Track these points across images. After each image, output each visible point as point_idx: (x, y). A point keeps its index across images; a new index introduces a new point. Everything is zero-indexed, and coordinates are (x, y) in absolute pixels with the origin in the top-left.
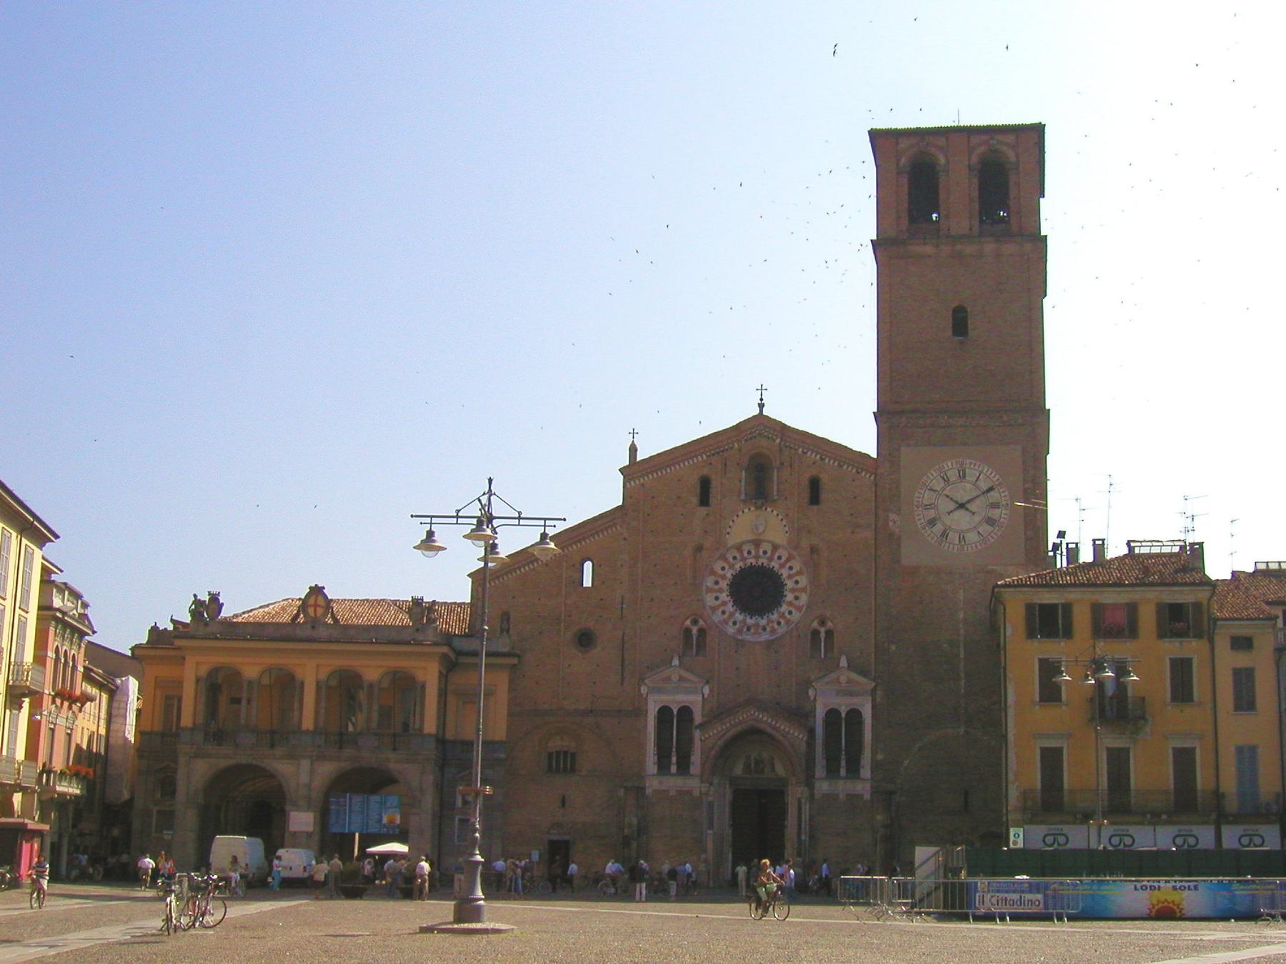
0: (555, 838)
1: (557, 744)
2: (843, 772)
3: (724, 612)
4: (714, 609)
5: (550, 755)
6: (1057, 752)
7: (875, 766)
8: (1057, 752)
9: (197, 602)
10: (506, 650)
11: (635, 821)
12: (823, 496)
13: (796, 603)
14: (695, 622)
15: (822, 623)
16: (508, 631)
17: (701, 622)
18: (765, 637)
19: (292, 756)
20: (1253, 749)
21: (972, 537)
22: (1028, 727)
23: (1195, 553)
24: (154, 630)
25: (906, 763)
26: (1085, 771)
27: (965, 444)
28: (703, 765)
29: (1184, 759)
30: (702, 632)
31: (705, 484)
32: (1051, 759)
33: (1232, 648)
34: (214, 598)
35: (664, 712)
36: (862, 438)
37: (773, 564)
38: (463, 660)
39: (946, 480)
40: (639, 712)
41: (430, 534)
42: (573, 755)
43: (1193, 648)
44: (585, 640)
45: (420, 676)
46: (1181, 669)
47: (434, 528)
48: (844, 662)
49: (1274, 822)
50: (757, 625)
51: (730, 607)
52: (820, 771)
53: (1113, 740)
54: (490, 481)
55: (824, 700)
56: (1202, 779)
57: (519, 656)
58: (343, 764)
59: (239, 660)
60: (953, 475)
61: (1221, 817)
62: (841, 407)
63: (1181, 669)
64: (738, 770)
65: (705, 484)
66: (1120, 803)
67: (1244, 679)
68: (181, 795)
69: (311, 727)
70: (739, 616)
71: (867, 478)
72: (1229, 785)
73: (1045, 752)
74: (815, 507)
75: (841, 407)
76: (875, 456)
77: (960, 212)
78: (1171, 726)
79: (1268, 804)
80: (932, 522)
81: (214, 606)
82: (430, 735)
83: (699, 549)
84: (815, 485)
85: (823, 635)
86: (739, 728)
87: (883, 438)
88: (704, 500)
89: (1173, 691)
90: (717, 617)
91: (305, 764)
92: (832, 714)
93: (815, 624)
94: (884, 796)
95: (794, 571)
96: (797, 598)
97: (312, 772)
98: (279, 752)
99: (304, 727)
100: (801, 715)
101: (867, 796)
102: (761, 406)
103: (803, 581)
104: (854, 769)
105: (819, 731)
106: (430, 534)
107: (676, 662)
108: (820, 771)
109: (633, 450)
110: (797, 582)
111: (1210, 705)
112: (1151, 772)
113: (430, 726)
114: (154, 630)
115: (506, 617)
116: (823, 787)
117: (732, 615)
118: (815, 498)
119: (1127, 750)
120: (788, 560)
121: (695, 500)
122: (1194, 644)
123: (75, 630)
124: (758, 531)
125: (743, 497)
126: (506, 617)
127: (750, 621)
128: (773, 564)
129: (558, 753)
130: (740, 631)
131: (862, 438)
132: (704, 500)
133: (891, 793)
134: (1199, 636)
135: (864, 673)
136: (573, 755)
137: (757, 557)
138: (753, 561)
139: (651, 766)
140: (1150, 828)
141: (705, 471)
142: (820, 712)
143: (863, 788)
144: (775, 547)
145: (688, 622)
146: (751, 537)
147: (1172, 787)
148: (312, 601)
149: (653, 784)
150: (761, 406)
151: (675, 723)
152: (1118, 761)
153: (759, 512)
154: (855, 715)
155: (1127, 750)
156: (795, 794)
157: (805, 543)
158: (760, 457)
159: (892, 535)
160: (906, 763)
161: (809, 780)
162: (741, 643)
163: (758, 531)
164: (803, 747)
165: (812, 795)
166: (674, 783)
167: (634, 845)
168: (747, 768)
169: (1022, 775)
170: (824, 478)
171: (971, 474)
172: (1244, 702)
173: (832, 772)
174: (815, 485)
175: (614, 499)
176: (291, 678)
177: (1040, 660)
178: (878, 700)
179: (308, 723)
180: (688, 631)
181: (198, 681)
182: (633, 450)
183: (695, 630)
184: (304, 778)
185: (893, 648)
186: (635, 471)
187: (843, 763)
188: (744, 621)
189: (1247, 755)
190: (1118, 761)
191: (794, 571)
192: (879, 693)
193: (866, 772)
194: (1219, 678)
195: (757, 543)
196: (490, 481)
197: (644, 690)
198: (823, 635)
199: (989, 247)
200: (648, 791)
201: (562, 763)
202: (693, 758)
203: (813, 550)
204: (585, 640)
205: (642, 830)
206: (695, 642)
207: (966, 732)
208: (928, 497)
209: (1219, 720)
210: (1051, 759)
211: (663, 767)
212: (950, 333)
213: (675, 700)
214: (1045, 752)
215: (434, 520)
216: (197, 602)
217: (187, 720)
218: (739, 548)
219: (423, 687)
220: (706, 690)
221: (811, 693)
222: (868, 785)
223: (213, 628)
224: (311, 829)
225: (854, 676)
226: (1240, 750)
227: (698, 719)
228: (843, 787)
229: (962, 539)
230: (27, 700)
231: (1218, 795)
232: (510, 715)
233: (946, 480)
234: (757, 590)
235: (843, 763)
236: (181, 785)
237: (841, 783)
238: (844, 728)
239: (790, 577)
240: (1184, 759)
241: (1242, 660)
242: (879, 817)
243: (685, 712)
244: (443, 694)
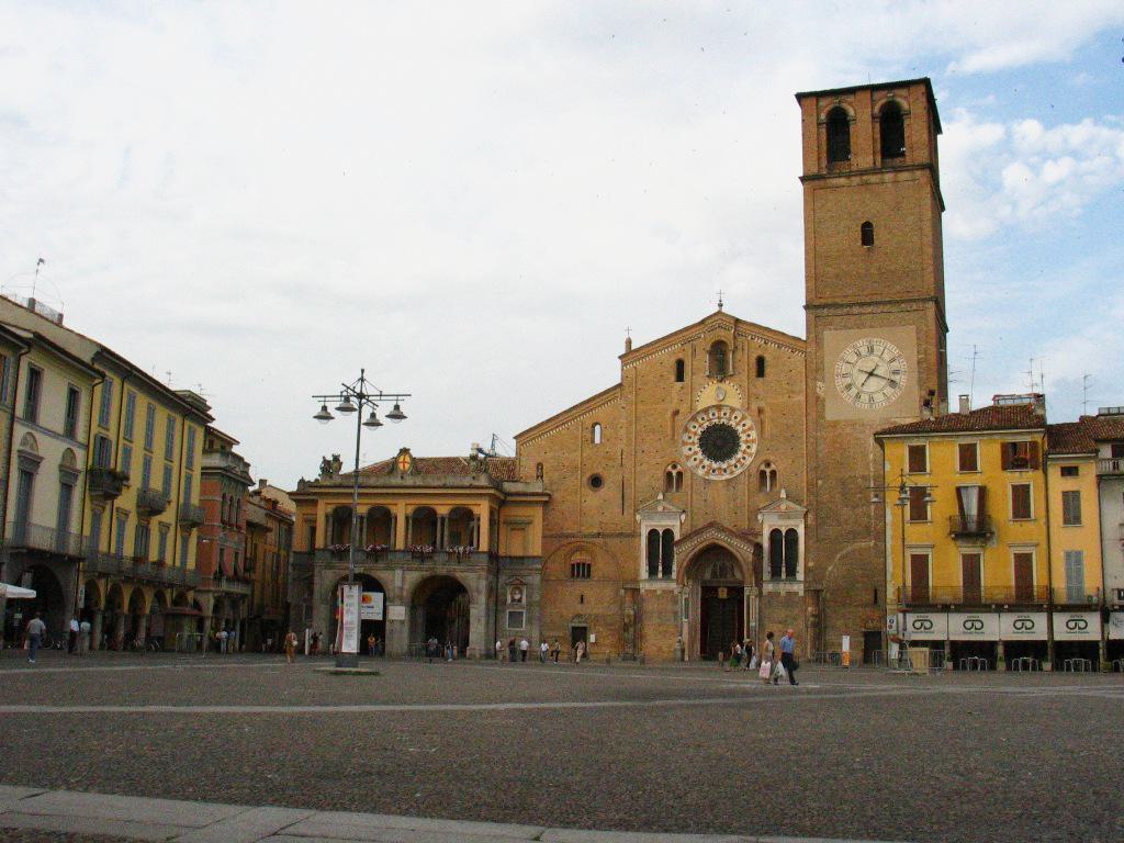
0: (577, 625)
1: (577, 558)
2: (783, 576)
3: (695, 459)
4: (688, 458)
5: (573, 565)
6: (1028, 556)
7: (807, 570)
8: (1028, 556)
9: (325, 462)
10: (540, 491)
11: (632, 613)
12: (767, 370)
13: (748, 451)
14: (674, 467)
15: (768, 465)
16: (542, 477)
17: (679, 467)
18: (727, 476)
19: (390, 568)
20: (1079, 554)
21: (879, 397)
22: (902, 540)
23: (210, 408)
24: (302, 482)
25: (830, 569)
26: (947, 574)
27: (871, 327)
28: (678, 573)
29: (1023, 563)
30: (680, 474)
31: (680, 364)
32: (920, 564)
33: (1063, 475)
34: (336, 458)
35: (653, 533)
36: (794, 323)
37: (731, 422)
38: (509, 498)
39: (859, 354)
40: (635, 535)
41: (397, 407)
42: (589, 565)
43: (1028, 477)
44: (596, 482)
45: (476, 510)
46: (1021, 494)
47: (327, 404)
48: (783, 495)
49: (1095, 611)
50: (720, 469)
51: (700, 456)
52: (766, 576)
53: (969, 550)
54: (363, 371)
55: (768, 523)
56: (1038, 579)
57: (549, 495)
58: (424, 573)
59: (389, 501)
60: (864, 351)
61: (1052, 608)
62: (778, 302)
63: (1021, 494)
64: (708, 576)
65: (680, 364)
66: (972, 601)
67: (1071, 501)
68: (317, 596)
69: (486, 549)
70: (706, 462)
71: (799, 358)
72: (1060, 584)
73: (1018, 557)
74: (761, 379)
75: (778, 302)
76: (804, 338)
77: (871, 140)
78: (1014, 535)
79: (1090, 597)
80: (849, 387)
81: (336, 465)
82: (484, 552)
83: (676, 413)
84: (761, 361)
85: (768, 474)
86: (704, 544)
87: (811, 326)
88: (680, 377)
89: (1014, 513)
90: (691, 463)
91: (399, 573)
92: (775, 533)
93: (763, 467)
94: (815, 594)
95: (746, 427)
96: (749, 447)
97: (403, 579)
98: (381, 565)
99: (397, 548)
100: (750, 536)
101: (801, 593)
102: (721, 305)
103: (754, 434)
104: (792, 572)
105: (766, 544)
106: (397, 407)
107: (660, 497)
108: (766, 576)
109: (629, 342)
110: (749, 436)
111: (1044, 520)
112: (997, 574)
113: (484, 546)
114: (302, 482)
115: (540, 466)
116: (768, 587)
117: (701, 461)
118: (761, 372)
119: (979, 555)
120: (743, 419)
121: (673, 378)
122: (1030, 473)
123: (237, 482)
124: (717, 397)
125: (707, 373)
126: (540, 466)
127: (715, 466)
128: (731, 422)
129: (578, 564)
130: (707, 473)
131: (794, 323)
132: (680, 377)
133: (818, 591)
134: (1035, 468)
135: (798, 502)
136: (589, 565)
137: (719, 418)
138: (716, 421)
139: (644, 573)
140: (996, 615)
141: (680, 356)
142: (644, 532)
143: (799, 588)
144: (733, 410)
145: (670, 467)
146: (714, 403)
147: (1013, 583)
148: (401, 459)
149: (644, 587)
150: (721, 305)
151: (662, 546)
152: (971, 567)
153: (720, 385)
154: (792, 533)
155: (979, 555)
156: (749, 592)
157: (754, 407)
158: (721, 344)
159: (818, 398)
160: (830, 569)
161: (759, 582)
162: (707, 482)
163: (717, 397)
164: (751, 558)
165: (761, 593)
166: (659, 586)
167: (631, 630)
168: (714, 574)
169: (898, 577)
170: (768, 358)
171: (878, 349)
172: (1072, 516)
173: (775, 573)
174: (761, 361)
175: (614, 378)
176: (388, 513)
177: (1014, 487)
178: (809, 522)
179: (400, 545)
180: (669, 474)
181: (327, 516)
182: (629, 342)
183: (674, 473)
184: (398, 583)
185: (820, 482)
186: (630, 355)
187: (784, 569)
188: (710, 466)
189: (1074, 559)
190: (971, 567)
191: (746, 427)
192: (810, 516)
193: (800, 576)
194: (1051, 501)
195: (719, 407)
196: (363, 371)
197: (638, 517)
198: (768, 474)
199: (888, 177)
200: (642, 591)
201: (582, 571)
202: (798, 568)
203: (760, 411)
204: (596, 482)
205: (638, 618)
206: (673, 480)
207: (875, 544)
208: (845, 368)
209: (1052, 534)
210: (920, 564)
211: (652, 571)
212: (860, 243)
213: (661, 524)
214: (1018, 557)
215: (327, 399)
216: (325, 462)
217: (320, 542)
218: (706, 411)
219: (479, 519)
220: (683, 517)
221: (760, 517)
222: (802, 586)
223: (337, 480)
224: (403, 618)
225: (791, 504)
226: (1068, 555)
227: (677, 537)
228: (783, 588)
229: (871, 399)
230: (195, 529)
231: (1050, 591)
232: (544, 537)
233: (859, 354)
234: (719, 442)
235: (784, 569)
236: (317, 588)
237: (781, 585)
238: (784, 543)
239: (744, 432)
240: (1023, 563)
241: (1070, 484)
242: (810, 609)
243: (668, 533)
244: (492, 522)
